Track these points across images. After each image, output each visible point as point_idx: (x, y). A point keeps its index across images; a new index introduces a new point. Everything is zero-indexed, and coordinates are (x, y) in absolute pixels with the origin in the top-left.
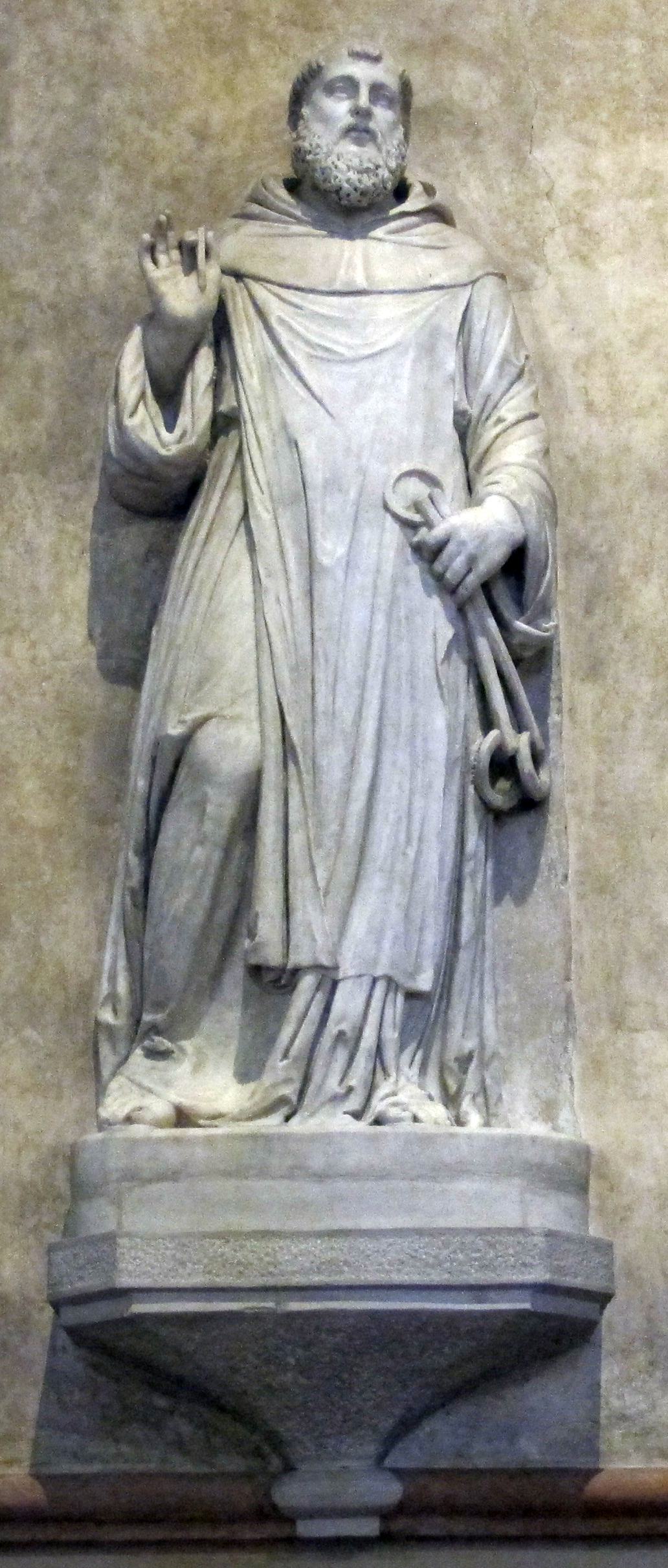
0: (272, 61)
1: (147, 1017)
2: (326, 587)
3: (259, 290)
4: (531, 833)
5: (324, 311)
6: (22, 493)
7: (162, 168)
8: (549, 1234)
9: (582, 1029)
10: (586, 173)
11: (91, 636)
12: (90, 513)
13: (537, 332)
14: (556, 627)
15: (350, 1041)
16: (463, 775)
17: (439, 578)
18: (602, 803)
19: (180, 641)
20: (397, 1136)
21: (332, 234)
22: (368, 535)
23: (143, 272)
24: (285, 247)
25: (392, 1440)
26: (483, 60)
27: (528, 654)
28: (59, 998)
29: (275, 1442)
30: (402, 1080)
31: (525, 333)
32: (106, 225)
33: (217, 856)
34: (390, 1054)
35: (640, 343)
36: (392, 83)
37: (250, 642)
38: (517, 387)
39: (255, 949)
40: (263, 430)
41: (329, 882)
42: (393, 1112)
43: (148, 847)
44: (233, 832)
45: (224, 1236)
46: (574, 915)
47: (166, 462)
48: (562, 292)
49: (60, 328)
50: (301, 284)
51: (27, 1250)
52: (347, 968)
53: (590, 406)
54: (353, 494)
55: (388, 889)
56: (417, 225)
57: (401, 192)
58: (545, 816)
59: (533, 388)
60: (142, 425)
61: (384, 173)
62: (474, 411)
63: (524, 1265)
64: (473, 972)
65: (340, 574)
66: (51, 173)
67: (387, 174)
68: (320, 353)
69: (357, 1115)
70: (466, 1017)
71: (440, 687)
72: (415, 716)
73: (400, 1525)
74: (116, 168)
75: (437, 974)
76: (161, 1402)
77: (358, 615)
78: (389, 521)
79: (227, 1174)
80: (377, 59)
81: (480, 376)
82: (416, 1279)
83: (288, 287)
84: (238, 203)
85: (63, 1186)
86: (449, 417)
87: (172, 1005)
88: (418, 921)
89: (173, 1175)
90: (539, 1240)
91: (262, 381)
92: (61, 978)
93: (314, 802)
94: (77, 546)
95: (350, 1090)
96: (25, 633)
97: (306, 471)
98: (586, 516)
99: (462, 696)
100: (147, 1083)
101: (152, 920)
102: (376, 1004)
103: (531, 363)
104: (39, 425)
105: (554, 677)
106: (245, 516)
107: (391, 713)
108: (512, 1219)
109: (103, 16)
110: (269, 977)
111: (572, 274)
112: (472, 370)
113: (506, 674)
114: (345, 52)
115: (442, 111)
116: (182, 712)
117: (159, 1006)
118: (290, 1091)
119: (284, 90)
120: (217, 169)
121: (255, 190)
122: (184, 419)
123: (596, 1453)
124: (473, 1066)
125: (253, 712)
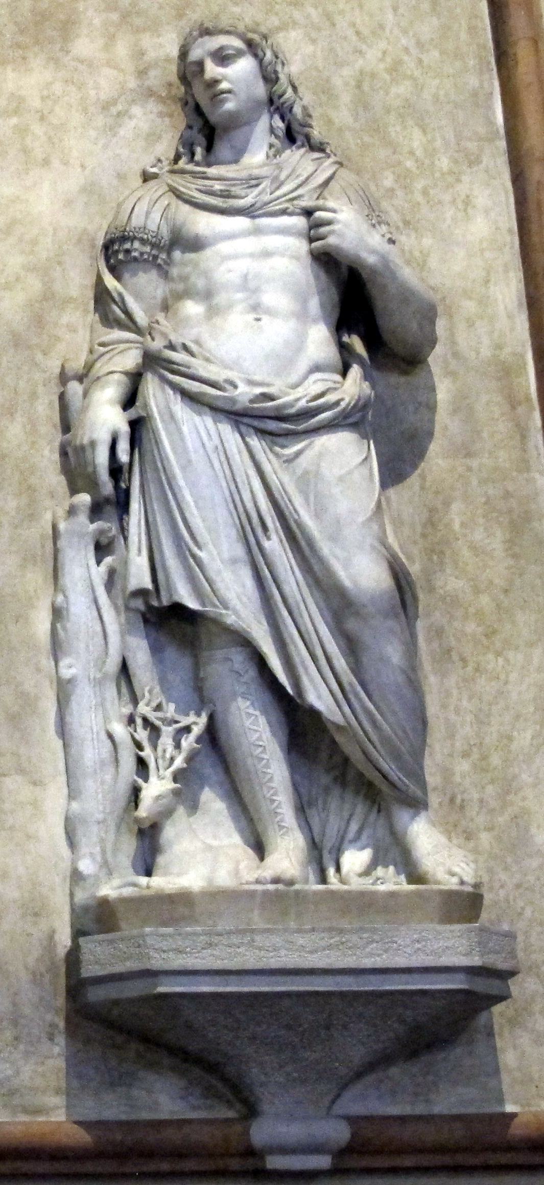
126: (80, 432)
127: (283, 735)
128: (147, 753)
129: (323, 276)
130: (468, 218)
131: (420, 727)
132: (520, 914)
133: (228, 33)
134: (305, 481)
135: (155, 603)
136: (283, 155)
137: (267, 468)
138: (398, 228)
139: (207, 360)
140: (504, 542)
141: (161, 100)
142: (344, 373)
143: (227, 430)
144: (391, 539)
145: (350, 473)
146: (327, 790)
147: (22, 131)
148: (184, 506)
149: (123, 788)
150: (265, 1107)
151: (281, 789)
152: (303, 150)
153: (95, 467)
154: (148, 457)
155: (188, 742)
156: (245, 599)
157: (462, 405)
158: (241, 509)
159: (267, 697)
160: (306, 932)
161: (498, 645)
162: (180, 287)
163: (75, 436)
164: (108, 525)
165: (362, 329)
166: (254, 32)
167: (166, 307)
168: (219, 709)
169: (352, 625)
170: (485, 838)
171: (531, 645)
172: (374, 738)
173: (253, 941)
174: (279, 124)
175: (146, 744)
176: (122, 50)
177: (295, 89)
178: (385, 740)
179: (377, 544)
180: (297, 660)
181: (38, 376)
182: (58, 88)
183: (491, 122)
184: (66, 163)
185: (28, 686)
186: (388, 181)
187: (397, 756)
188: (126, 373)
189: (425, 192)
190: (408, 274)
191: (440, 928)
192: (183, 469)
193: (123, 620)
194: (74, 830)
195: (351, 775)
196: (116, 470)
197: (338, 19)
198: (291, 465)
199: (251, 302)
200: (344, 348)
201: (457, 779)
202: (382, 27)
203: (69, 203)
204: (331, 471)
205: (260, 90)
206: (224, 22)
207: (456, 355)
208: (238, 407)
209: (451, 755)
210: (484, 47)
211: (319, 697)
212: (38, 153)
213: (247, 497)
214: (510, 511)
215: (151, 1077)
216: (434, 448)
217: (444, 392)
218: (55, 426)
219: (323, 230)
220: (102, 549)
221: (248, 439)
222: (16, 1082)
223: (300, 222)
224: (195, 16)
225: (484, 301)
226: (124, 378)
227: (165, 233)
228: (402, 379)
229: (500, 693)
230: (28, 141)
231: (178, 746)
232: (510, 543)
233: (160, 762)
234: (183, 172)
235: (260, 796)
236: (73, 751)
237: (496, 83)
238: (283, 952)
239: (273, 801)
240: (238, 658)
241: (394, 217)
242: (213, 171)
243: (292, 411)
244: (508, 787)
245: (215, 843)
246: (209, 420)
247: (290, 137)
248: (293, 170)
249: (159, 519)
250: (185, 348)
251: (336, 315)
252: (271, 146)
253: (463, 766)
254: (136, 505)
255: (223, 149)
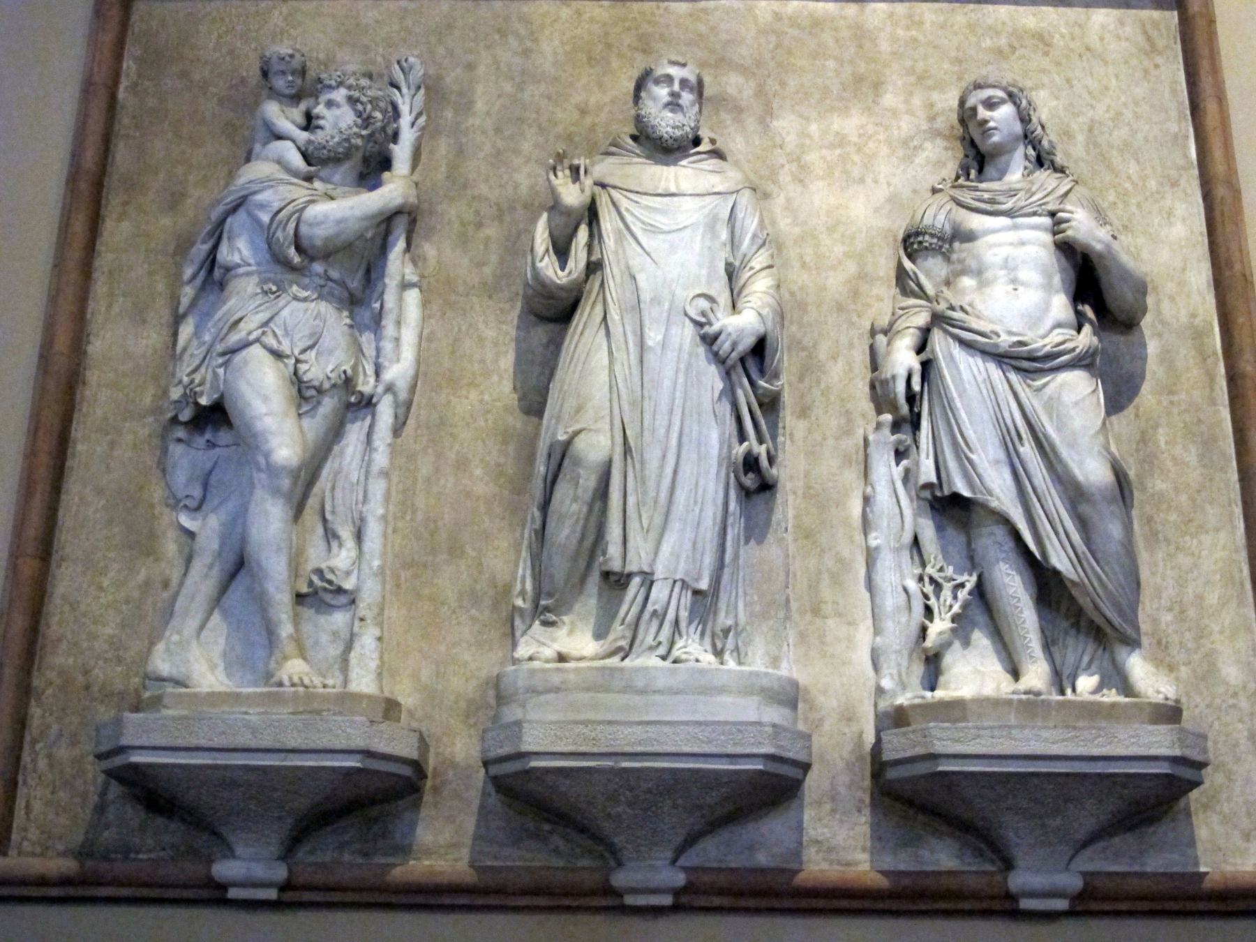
0: (625, 70)
1: (543, 602)
2: (650, 358)
3: (614, 193)
4: (767, 503)
5: (651, 204)
6: (477, 307)
7: (560, 129)
8: (774, 726)
9: (796, 616)
10: (803, 134)
11: (515, 388)
12: (516, 319)
13: (774, 223)
14: (783, 385)
15: (660, 616)
16: (727, 468)
17: (716, 354)
18: (809, 488)
19: (566, 388)
20: (688, 669)
21: (657, 162)
22: (675, 330)
23: (548, 180)
24: (630, 170)
25: (680, 851)
26: (743, 70)
27: (767, 400)
28: (491, 592)
29: (613, 850)
30: (690, 641)
31: (767, 221)
32: (528, 160)
33: (585, 509)
34: (683, 625)
35: (831, 230)
36: (692, 79)
37: (607, 388)
38: (761, 251)
39: (606, 562)
40: (616, 271)
41: (649, 525)
42: (684, 657)
43: (545, 506)
44: (594, 495)
45: (585, 723)
46: (792, 549)
47: (560, 288)
48: (788, 200)
49: (500, 218)
50: (639, 190)
51: (470, 737)
52: (659, 573)
53: (804, 265)
54: (667, 305)
55: (683, 530)
56: (707, 159)
57: (697, 141)
58: (775, 494)
59: (770, 252)
60: (547, 266)
61: (687, 129)
62: (737, 264)
63: (760, 743)
64: (732, 580)
65: (659, 352)
66: (498, 130)
67: (689, 129)
68: (649, 228)
69: (664, 658)
70: (728, 606)
71: (715, 416)
72: (700, 433)
73: (684, 900)
74: (534, 130)
75: (711, 580)
76: (547, 827)
77: (669, 372)
78: (687, 321)
79: (588, 690)
80: (684, 65)
81: (741, 243)
82: (696, 750)
83: (631, 191)
84: (603, 149)
85: (493, 702)
86: (722, 266)
87: (557, 596)
88: (701, 550)
89: (557, 690)
90: (769, 730)
91: (616, 243)
92: (493, 583)
93: (642, 481)
94: (508, 338)
95: (660, 643)
96: (477, 386)
97: (640, 293)
98: (801, 326)
99: (728, 422)
100: (542, 639)
101: (547, 545)
102: (675, 595)
103: (770, 237)
104: (487, 270)
105: (781, 415)
106: (605, 318)
107: (686, 430)
108: (753, 717)
109: (529, 44)
110: (613, 578)
111: (793, 190)
112: (736, 240)
113: (753, 409)
114: (665, 61)
115: (721, 101)
116: (566, 427)
117: (550, 595)
118: (624, 643)
119: (631, 86)
120: (592, 128)
121: (614, 139)
122: (571, 264)
123: (801, 863)
124: (731, 634)
125: (608, 427)
126: (885, 369)
127: (1034, 590)
128: (933, 602)
129: (1063, 259)
130: (1171, 224)
131: (1135, 586)
132: (1211, 726)
133: (994, 87)
134: (1050, 406)
135: (938, 494)
136: (1035, 175)
137: (1022, 395)
138: (1119, 230)
139: (978, 317)
140: (1198, 455)
141: (945, 138)
142: (1079, 330)
143: (992, 368)
144: (1113, 448)
145: (1083, 399)
146: (1066, 633)
147: (844, 159)
148: (960, 422)
149: (914, 629)
150: (1020, 863)
151: (1031, 629)
152: (1049, 171)
153: (895, 394)
154: (934, 388)
155: (963, 594)
156: (1005, 491)
157: (1166, 357)
158: (1003, 425)
159: (1021, 562)
160: (1049, 728)
161: (1193, 530)
162: (959, 267)
163: (881, 373)
164: (905, 437)
165: (1092, 301)
166: (1014, 86)
167: (948, 283)
168: (985, 571)
169: (1084, 508)
170: (1184, 671)
171: (1217, 530)
172: (1100, 590)
173: (1010, 733)
174: (1031, 152)
175: (932, 596)
176: (917, 101)
177: (1043, 127)
178: (1109, 594)
179: (1102, 450)
180: (1043, 534)
181: (854, 333)
182: (870, 129)
183: (1186, 156)
184: (876, 182)
185: (846, 553)
186: (1112, 197)
187: (1121, 612)
188: (919, 328)
189: (1139, 205)
190: (1125, 258)
191: (1150, 727)
192: (960, 396)
193: (915, 507)
194: (878, 658)
195: (1083, 623)
196: (911, 398)
197: (1075, 82)
198: (1041, 393)
199: (1011, 277)
200: (1078, 313)
201: (1163, 626)
202: (1107, 88)
203: (877, 210)
204: (1068, 398)
205: (1018, 128)
206: (991, 80)
207: (1162, 322)
208: (1001, 350)
209: (1158, 609)
210: (1182, 103)
211: (1060, 560)
212: (856, 173)
213: (1007, 415)
214: (1202, 433)
215: (933, 841)
216: (1146, 388)
217: (1152, 347)
218: (866, 367)
219: (1064, 226)
220: (900, 455)
221: (1008, 374)
222: (834, 842)
223: (1047, 221)
224: (970, 78)
225: (1182, 283)
226: (917, 332)
227: (947, 228)
228: (1122, 338)
229: (1195, 565)
230: (849, 166)
231: (955, 597)
232: (1201, 456)
233: (942, 608)
234: (962, 186)
235: (1016, 634)
236: (878, 600)
237: (1191, 130)
238: (1033, 743)
239: (1026, 638)
240: (1000, 533)
241: (1116, 222)
242: (983, 186)
243: (1040, 354)
244: (1202, 634)
245: (983, 669)
246: (979, 361)
247: (1040, 162)
248: (1042, 185)
249: (940, 423)
250: (962, 308)
251: (1073, 289)
252: (1026, 168)
253: (1168, 617)
254: (925, 424)
255: (990, 170)
